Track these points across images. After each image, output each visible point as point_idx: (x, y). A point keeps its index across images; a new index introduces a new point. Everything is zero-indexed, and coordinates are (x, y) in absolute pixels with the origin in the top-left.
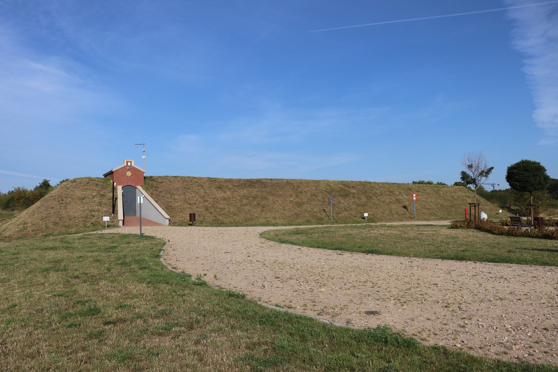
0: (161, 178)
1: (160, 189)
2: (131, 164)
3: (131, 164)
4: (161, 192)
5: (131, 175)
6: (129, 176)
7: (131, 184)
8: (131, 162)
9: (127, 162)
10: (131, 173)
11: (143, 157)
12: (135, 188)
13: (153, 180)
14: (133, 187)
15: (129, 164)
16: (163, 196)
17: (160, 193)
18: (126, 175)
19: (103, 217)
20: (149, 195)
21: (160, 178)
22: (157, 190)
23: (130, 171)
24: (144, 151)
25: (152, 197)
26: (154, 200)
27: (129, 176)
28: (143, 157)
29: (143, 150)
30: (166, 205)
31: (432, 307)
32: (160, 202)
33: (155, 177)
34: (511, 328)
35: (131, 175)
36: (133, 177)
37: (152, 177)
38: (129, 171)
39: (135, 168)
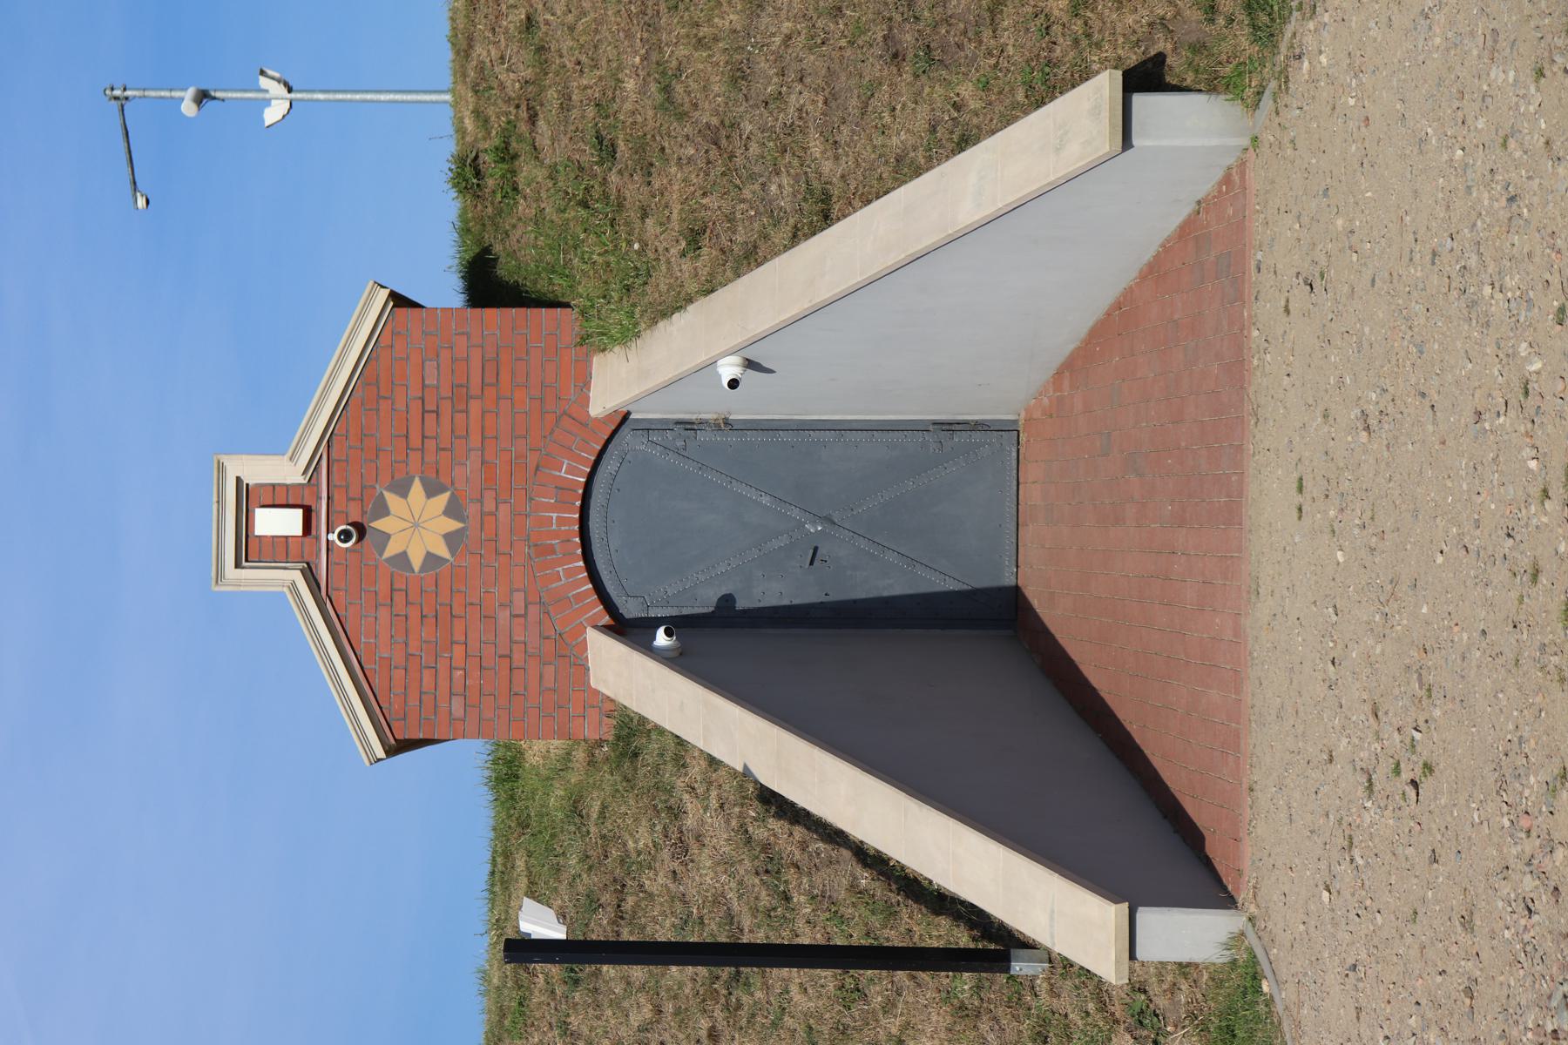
0: (470, 41)
1: (630, 84)
2: (278, 497)
3: (278, 497)
4: (667, 90)
5: (443, 499)
6: (453, 525)
7: (563, 488)
8: (249, 498)
9: (249, 549)
10: (403, 490)
11: (273, 114)
12: (626, 434)
13: (506, 155)
14: (609, 466)
15: (278, 523)
16: (739, 76)
17: (682, 116)
18: (431, 559)
19: (1127, 901)
20: (722, 295)
21: (479, 50)
22: (640, 148)
23: (383, 510)
24: (202, 97)
25: (752, 257)
26: (795, 238)
27: (453, 525)
28: (273, 114)
29: (188, 108)
30: (875, 68)
31: (1384, 636)
32: (816, 148)
33: (469, 124)
34: (844, 877)
35: (431, 491)
36: (472, 464)
37: (461, 161)
38: (380, 524)
39: (329, 439)
